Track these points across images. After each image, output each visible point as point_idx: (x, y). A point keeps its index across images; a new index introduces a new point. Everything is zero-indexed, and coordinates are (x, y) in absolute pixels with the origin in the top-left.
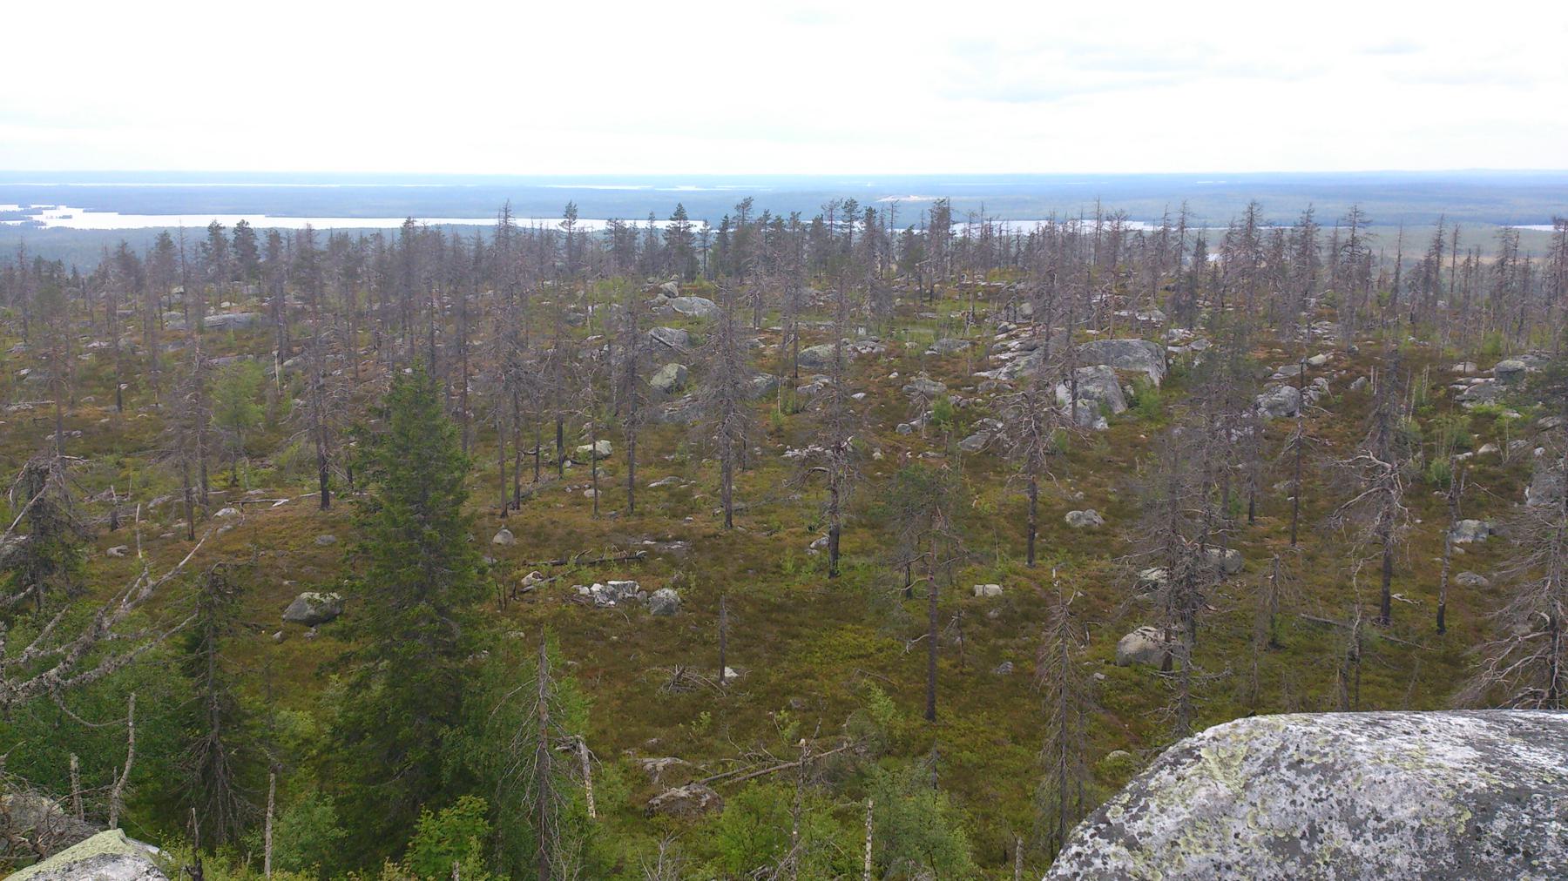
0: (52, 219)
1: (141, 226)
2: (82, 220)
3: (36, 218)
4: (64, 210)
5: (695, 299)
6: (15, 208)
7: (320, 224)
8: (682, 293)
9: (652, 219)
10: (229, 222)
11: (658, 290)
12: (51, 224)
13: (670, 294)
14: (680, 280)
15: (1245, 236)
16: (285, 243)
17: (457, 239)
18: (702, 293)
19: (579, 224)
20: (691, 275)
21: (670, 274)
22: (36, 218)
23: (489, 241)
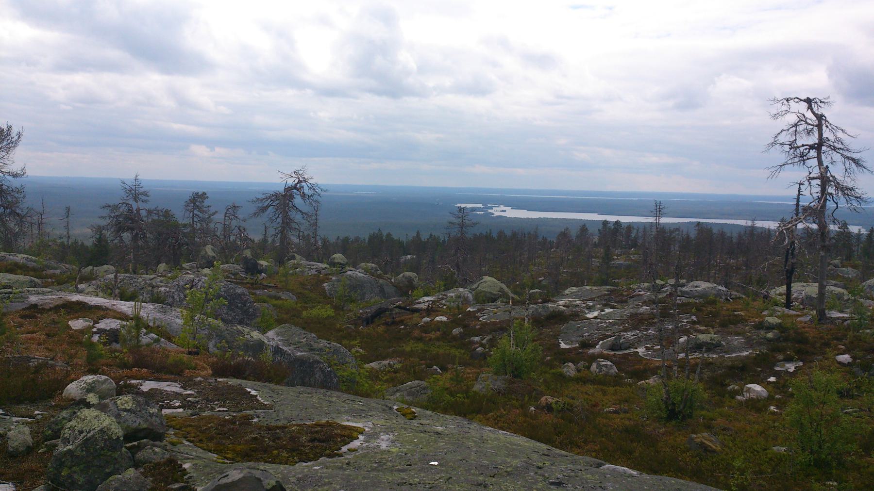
0: (496, 211)
1: (513, 216)
2: (511, 213)
3: (490, 211)
4: (502, 208)
5: (850, 269)
6: (481, 206)
7: (625, 219)
8: (843, 266)
9: (753, 220)
10: (612, 219)
11: (830, 264)
12: (497, 214)
13: (836, 266)
14: (842, 260)
15: (514, 235)
16: (635, 231)
17: (722, 234)
18: (854, 267)
19: (663, 220)
20: (849, 258)
21: (837, 256)
22: (490, 211)
23: (693, 234)
